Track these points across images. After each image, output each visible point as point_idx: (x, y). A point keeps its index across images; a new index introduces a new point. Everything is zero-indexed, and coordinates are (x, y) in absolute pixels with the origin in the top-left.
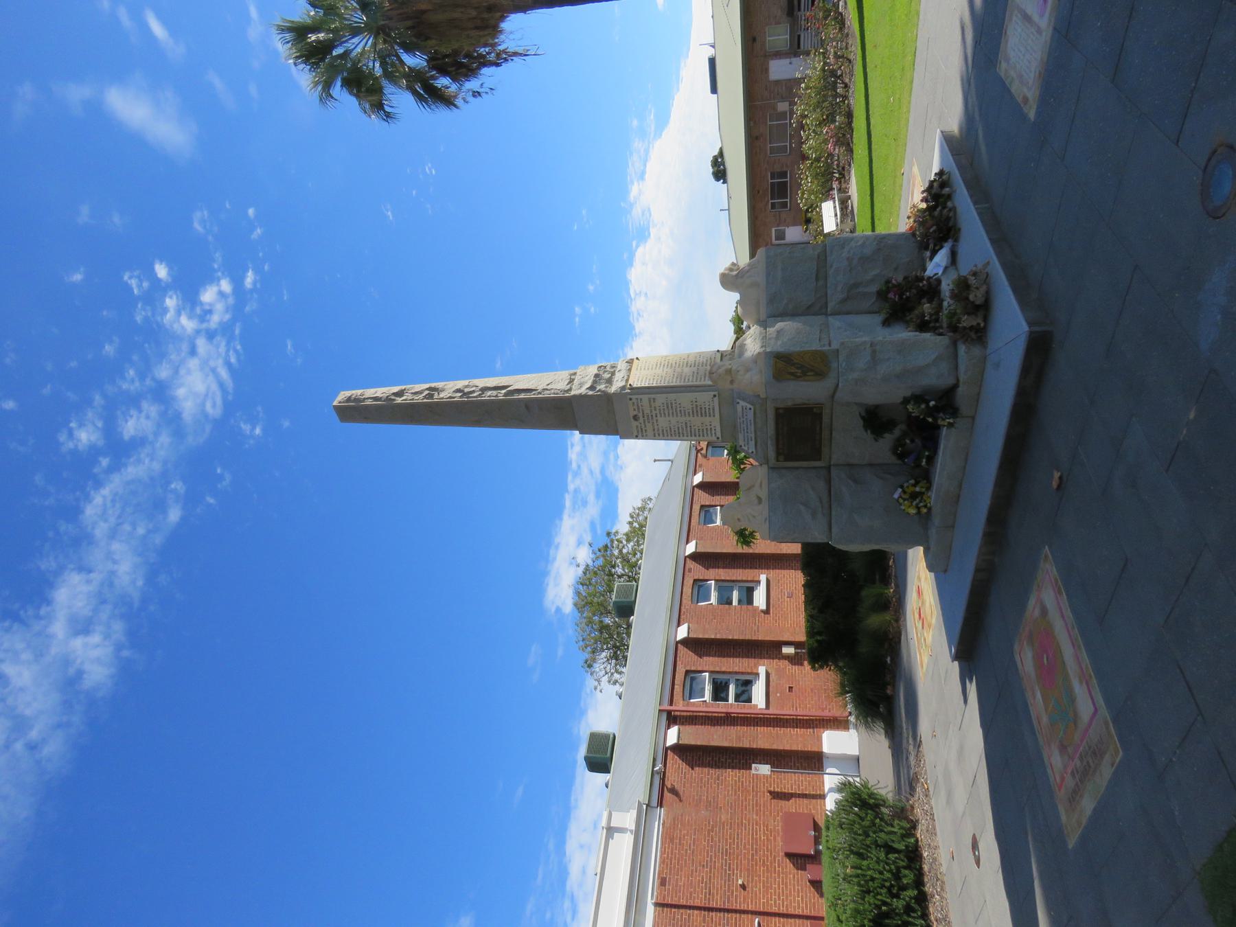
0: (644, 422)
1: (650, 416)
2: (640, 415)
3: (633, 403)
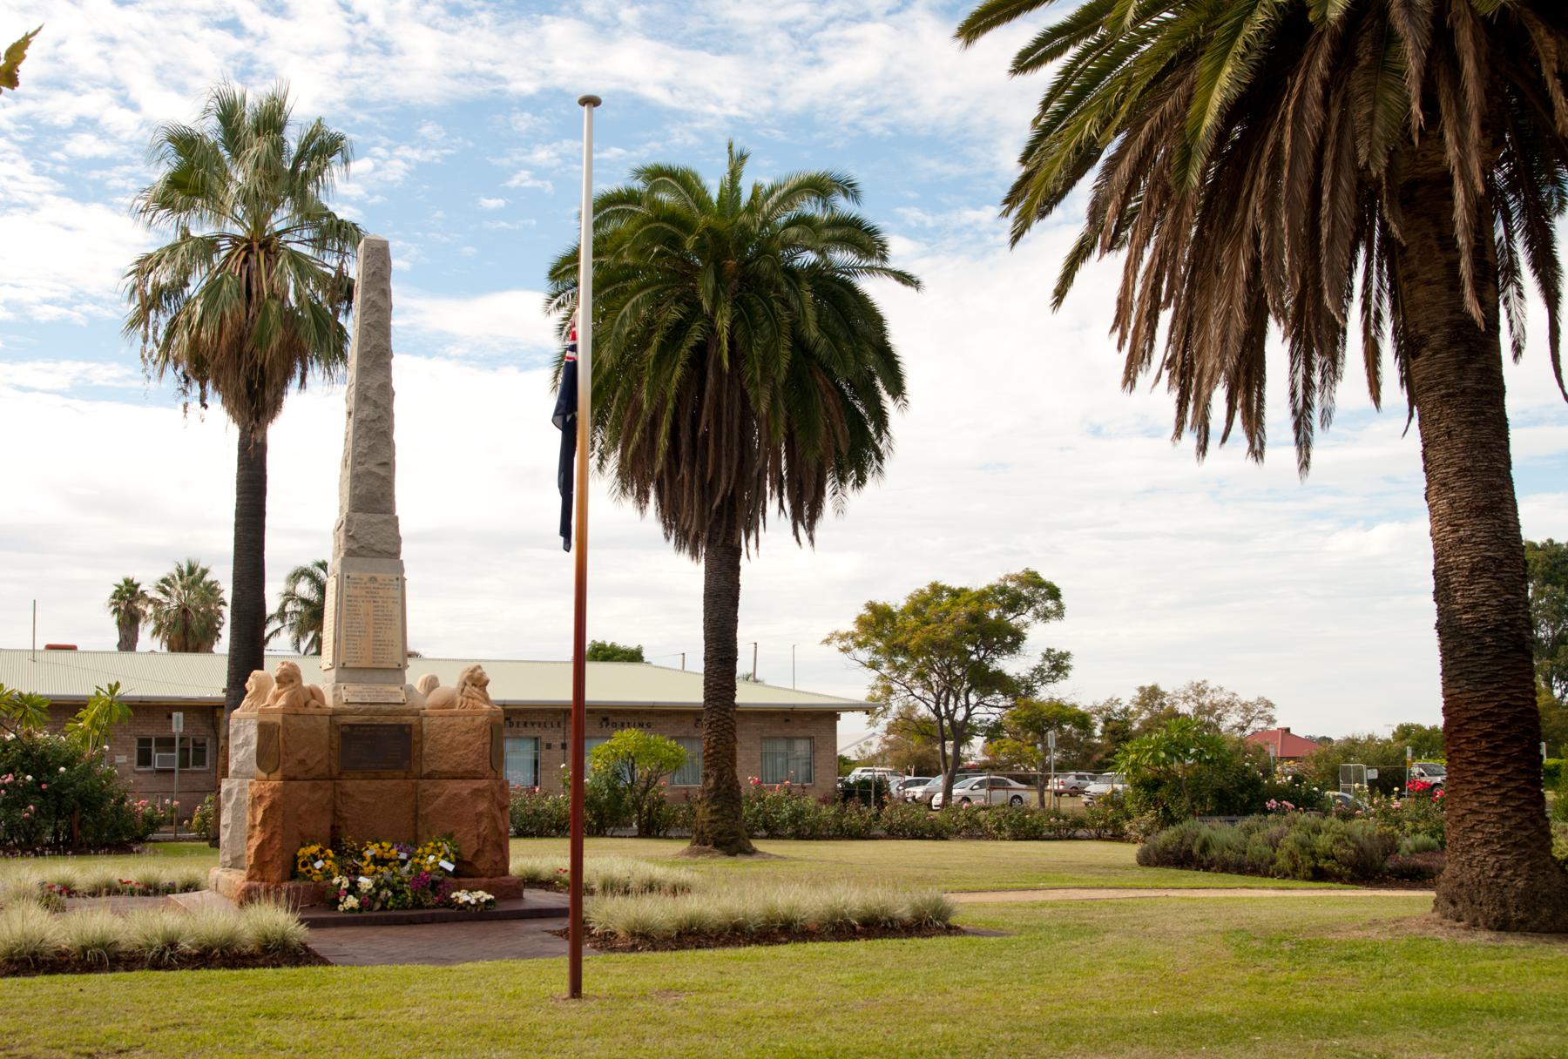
2: (377, 585)
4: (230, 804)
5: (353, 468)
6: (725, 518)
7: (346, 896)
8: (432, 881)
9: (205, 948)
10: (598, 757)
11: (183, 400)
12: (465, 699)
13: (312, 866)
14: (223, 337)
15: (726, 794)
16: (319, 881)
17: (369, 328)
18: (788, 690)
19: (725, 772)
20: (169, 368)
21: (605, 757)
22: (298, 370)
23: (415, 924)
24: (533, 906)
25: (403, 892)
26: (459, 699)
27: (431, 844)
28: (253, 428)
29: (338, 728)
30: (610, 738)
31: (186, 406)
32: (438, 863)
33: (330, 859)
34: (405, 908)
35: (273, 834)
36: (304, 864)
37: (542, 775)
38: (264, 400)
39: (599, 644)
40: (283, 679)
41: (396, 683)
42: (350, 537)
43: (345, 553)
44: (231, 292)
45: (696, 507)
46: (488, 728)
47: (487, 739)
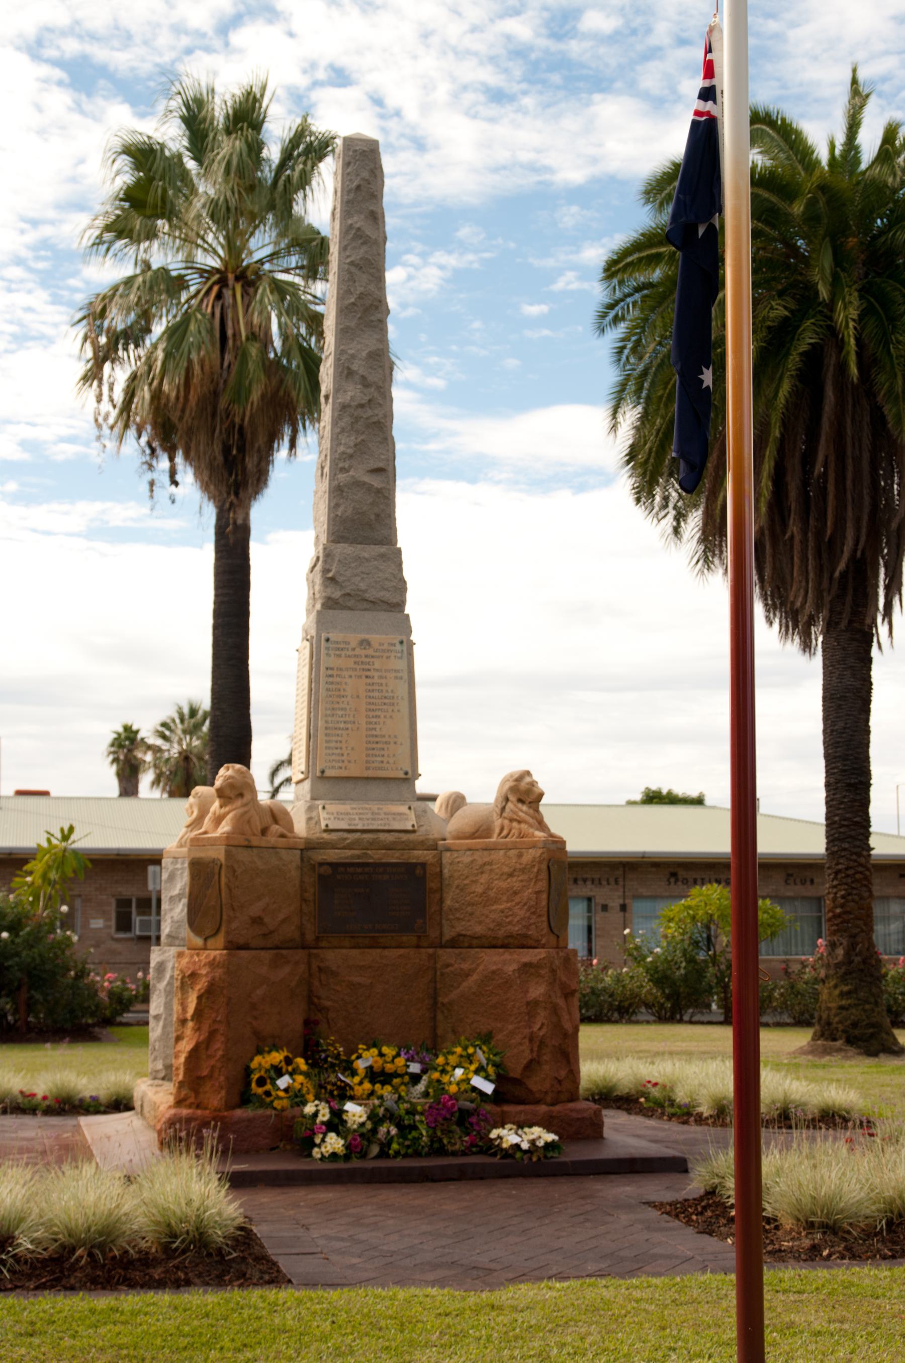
0: (355, 656)
1: (367, 667)
2: (370, 652)
3: (394, 645)
4: (162, 986)
5: (333, 477)
6: (850, 592)
7: (325, 1135)
8: (460, 1110)
9: (63, 1246)
10: (671, 920)
11: (149, 476)
12: (506, 822)
13: (274, 1084)
14: (192, 393)
15: (862, 971)
16: (283, 1109)
17: (353, 269)
18: (893, 836)
19: (859, 939)
20: (132, 433)
21: (680, 920)
22: (287, 431)
23: (434, 1181)
24: (622, 1153)
25: (414, 1127)
26: (498, 823)
27: (459, 1050)
28: (231, 504)
29: (313, 867)
30: (686, 896)
31: (152, 484)
32: (468, 1080)
33: (301, 1073)
34: (417, 1154)
35: (212, 1034)
36: (261, 1082)
37: (597, 944)
38: (244, 469)
39: (654, 792)
40: (228, 792)
41: (401, 800)
42: (330, 580)
43: (323, 605)
44: (200, 332)
45: (811, 575)
46: (544, 866)
47: (542, 885)
